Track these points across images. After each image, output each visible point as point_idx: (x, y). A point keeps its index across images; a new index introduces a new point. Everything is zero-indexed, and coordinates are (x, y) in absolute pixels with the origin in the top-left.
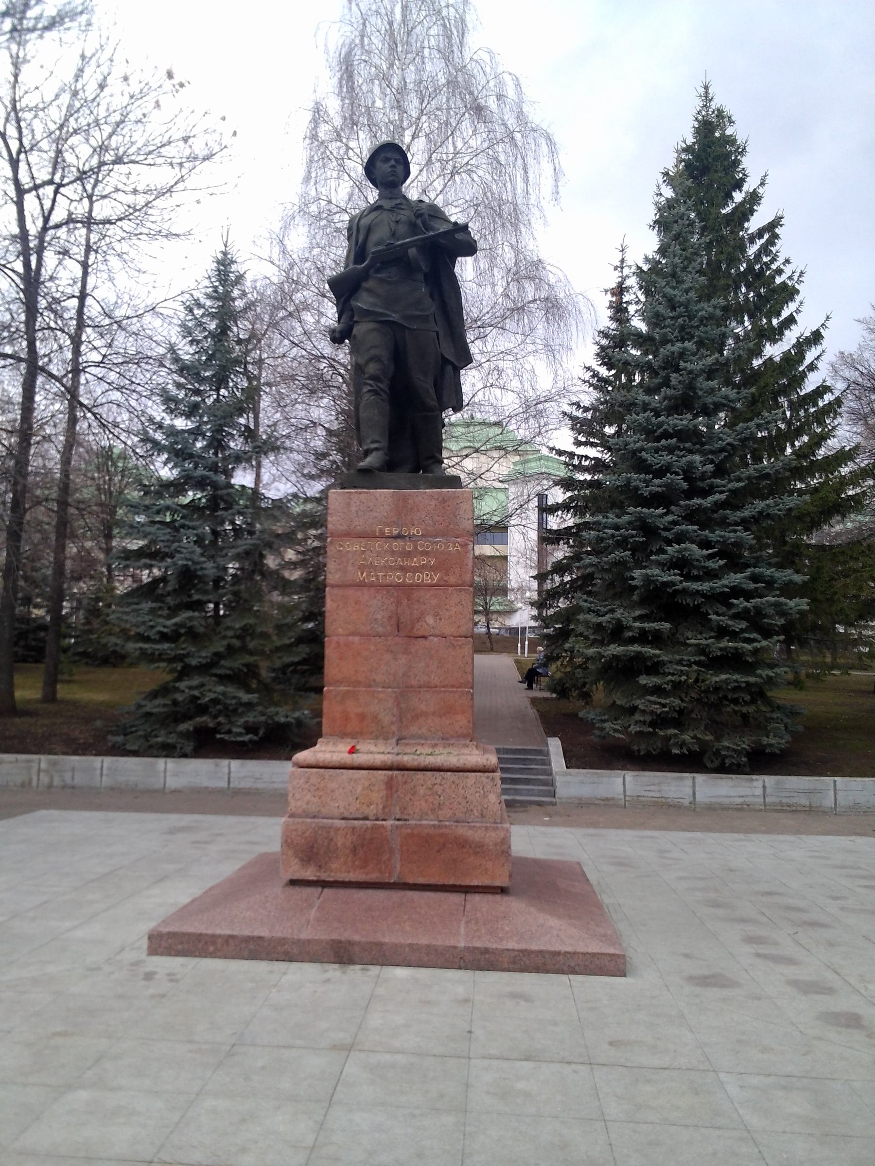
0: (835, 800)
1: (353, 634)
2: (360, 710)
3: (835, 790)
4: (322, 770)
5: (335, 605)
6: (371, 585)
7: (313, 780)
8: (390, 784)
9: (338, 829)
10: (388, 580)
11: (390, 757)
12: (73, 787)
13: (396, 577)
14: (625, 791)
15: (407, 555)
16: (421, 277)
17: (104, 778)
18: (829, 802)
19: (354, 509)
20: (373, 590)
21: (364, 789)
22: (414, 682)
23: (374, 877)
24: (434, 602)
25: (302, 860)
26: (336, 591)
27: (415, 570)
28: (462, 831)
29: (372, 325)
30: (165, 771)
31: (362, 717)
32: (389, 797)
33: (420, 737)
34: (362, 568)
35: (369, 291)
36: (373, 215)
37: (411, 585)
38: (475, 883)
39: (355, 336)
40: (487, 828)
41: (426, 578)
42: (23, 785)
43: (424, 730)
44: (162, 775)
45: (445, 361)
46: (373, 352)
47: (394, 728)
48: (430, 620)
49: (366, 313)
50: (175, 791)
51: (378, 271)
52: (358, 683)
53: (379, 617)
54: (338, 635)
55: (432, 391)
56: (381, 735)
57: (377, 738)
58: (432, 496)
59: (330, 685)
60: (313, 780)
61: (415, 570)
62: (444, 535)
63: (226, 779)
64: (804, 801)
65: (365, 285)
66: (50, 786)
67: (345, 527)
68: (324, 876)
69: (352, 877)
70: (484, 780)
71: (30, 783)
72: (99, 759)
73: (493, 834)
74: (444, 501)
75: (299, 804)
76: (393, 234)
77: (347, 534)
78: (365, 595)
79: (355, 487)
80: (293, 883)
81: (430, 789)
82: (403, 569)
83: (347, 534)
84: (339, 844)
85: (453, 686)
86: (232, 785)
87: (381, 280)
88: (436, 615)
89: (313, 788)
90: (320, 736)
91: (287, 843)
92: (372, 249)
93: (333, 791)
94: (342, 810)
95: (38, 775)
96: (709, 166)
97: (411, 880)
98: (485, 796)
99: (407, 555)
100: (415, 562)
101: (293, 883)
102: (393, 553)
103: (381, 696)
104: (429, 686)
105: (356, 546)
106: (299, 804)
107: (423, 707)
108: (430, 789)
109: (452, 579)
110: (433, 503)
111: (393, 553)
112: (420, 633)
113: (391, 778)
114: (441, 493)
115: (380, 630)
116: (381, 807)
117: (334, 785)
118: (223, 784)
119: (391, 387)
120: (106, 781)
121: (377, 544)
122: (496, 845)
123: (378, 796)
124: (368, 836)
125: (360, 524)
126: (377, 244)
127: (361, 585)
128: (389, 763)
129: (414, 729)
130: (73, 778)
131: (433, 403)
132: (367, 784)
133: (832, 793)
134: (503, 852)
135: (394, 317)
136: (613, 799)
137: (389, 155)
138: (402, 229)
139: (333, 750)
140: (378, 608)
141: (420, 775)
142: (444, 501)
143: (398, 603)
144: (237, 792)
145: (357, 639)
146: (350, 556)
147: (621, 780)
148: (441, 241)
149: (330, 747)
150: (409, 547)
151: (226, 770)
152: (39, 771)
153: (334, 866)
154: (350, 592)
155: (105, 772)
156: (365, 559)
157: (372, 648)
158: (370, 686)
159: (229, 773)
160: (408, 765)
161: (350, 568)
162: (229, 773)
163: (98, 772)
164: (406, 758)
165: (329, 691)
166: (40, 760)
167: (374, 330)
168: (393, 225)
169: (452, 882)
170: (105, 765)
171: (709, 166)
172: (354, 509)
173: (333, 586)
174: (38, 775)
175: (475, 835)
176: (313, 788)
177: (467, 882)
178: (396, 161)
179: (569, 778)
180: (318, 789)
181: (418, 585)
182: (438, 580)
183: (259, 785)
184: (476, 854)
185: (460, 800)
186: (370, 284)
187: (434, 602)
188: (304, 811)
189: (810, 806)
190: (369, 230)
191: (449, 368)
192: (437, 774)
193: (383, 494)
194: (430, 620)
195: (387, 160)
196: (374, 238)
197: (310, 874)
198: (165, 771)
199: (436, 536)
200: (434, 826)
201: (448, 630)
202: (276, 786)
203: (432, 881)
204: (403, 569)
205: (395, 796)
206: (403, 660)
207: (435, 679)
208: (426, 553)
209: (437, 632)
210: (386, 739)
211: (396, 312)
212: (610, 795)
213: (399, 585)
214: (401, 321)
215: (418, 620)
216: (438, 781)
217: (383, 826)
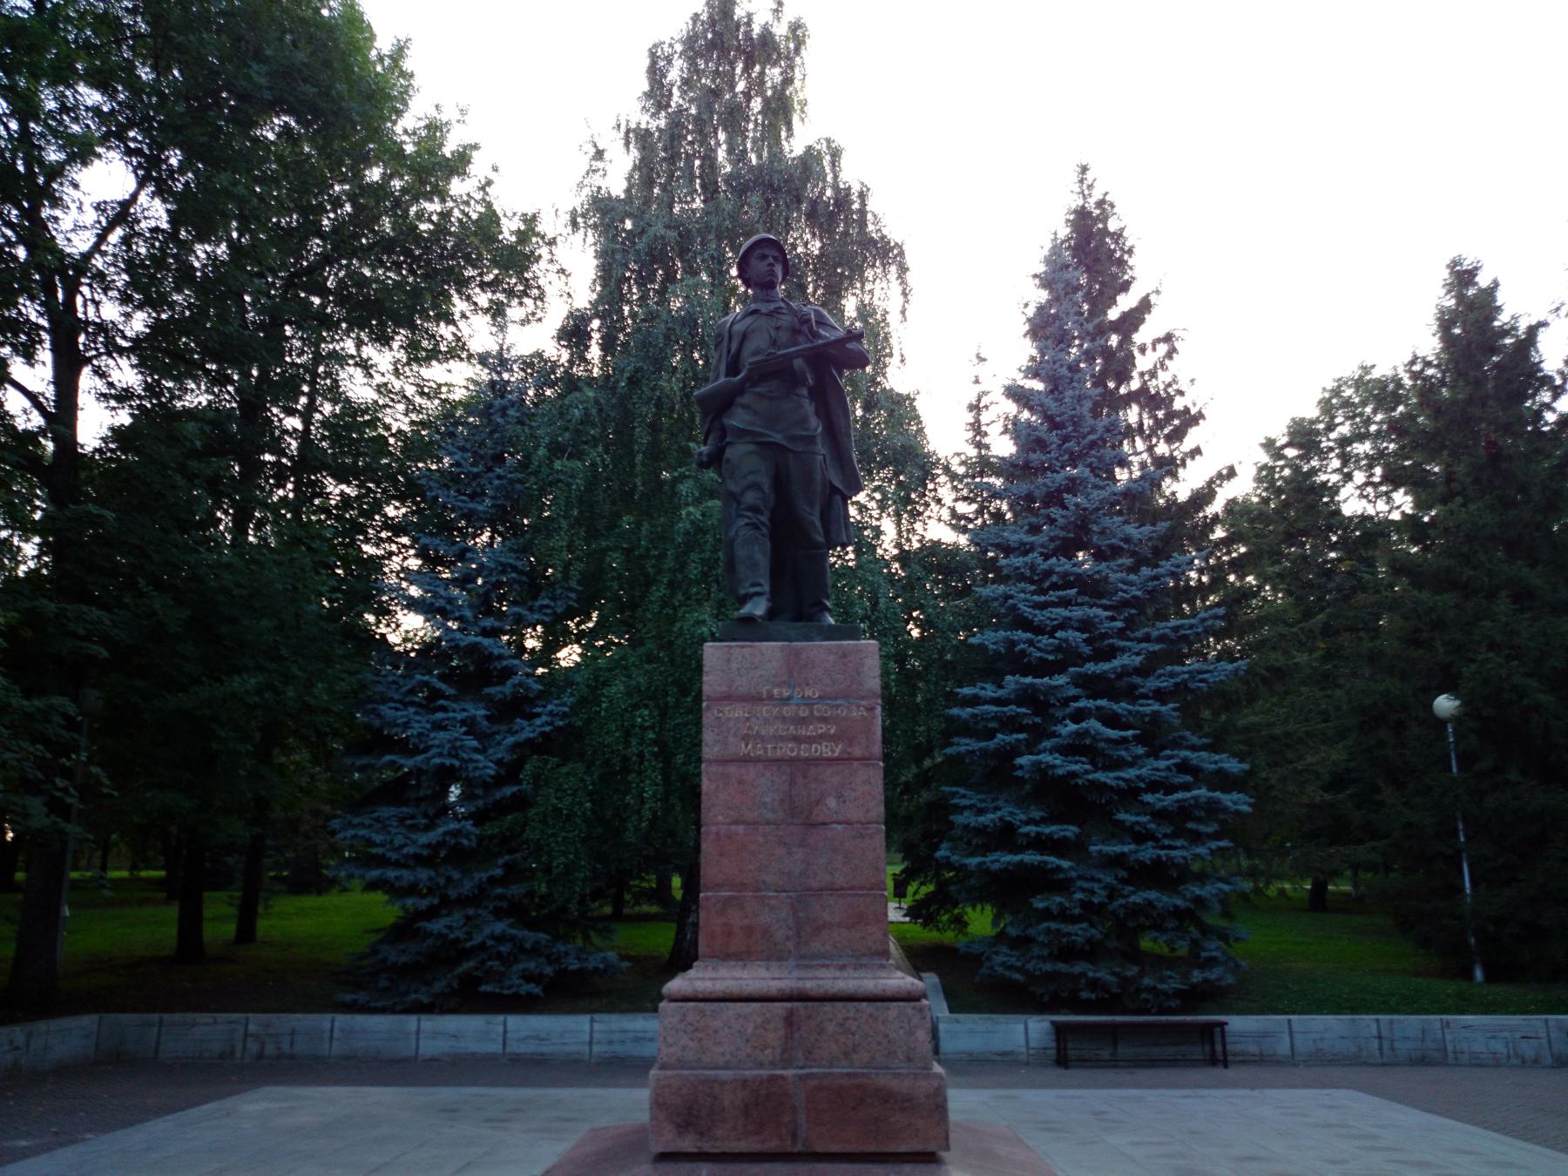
0: (1292, 1045)
1: (736, 822)
2: (746, 922)
3: (1291, 1033)
4: (701, 1005)
5: (713, 786)
6: (757, 760)
7: (691, 1018)
8: (789, 1021)
9: (723, 1083)
10: (779, 753)
11: (772, 983)
12: (292, 1057)
13: (787, 750)
14: (1027, 1041)
15: (803, 722)
16: (805, 392)
17: (335, 1043)
18: (1283, 1048)
19: (734, 666)
20: (760, 766)
21: (756, 1028)
22: (815, 884)
23: (772, 1145)
24: (836, 780)
25: (678, 1126)
26: (714, 769)
27: (810, 740)
28: (884, 1080)
29: (751, 447)
30: (418, 1031)
31: (749, 931)
32: (788, 1038)
33: (823, 956)
34: (746, 738)
35: (746, 407)
36: (749, 320)
37: (807, 759)
38: (903, 1148)
39: (728, 461)
40: (916, 1075)
41: (825, 750)
42: (221, 1056)
43: (828, 947)
44: (413, 1037)
45: (834, 490)
46: (751, 478)
47: (790, 945)
48: (832, 803)
49: (742, 433)
50: (432, 1059)
51: (754, 384)
52: (743, 886)
53: (768, 799)
54: (716, 824)
55: (818, 524)
56: (773, 955)
57: (768, 959)
58: (829, 651)
59: (708, 889)
60: (691, 1018)
61: (810, 740)
62: (845, 697)
63: (500, 1040)
64: (1253, 1049)
65: (739, 400)
66: (260, 1056)
67: (724, 689)
68: (707, 1147)
69: (743, 1146)
70: (910, 1011)
71: (232, 1053)
72: (328, 1017)
73: (924, 1083)
74: (844, 656)
75: (672, 1050)
76: (774, 343)
77: (728, 698)
78: (751, 772)
79: (734, 640)
80: (664, 1157)
81: (841, 1025)
82: (797, 739)
83: (728, 698)
84: (726, 1103)
85: (862, 888)
86: (508, 1050)
87: (760, 394)
88: (839, 797)
89: (690, 1029)
90: (696, 958)
91: (658, 1104)
92: (748, 359)
93: (716, 1032)
94: (728, 1057)
95: (245, 1042)
96: (1090, 259)
97: (819, 1148)
98: (911, 1033)
99: (803, 722)
100: (811, 731)
101: (664, 1157)
102: (784, 719)
103: (773, 902)
104: (832, 889)
105: (738, 712)
106: (672, 1050)
107: (826, 916)
108: (841, 1025)
109: (857, 752)
110: (831, 658)
111: (784, 719)
112: (820, 819)
113: (791, 1013)
114: (839, 647)
115: (770, 816)
116: (779, 1050)
117: (716, 1024)
118: (496, 1047)
119: (771, 520)
120: (337, 1049)
121: (764, 710)
122: (928, 1097)
123: (774, 1036)
124: (763, 1092)
125: (743, 685)
126: (756, 353)
127: (745, 760)
128: (788, 991)
129: (815, 946)
130: (292, 1044)
131: (821, 539)
132: (759, 1020)
133: (1286, 1038)
134: (938, 1106)
135: (778, 438)
136: (1012, 1053)
137: (766, 251)
138: (784, 336)
139: (714, 975)
140: (767, 788)
141: (827, 1007)
142: (844, 656)
143: (792, 783)
144: (517, 1060)
145: (741, 829)
146: (731, 724)
147: (1021, 1027)
148: (831, 351)
149: (710, 974)
150: (804, 712)
151: (501, 1029)
152: (246, 1034)
153: (719, 1133)
154: (732, 769)
155: (336, 1035)
156: (749, 728)
157: (760, 839)
158: (758, 890)
159: (505, 1032)
160: (813, 994)
161: (731, 739)
162: (505, 1032)
163: (327, 1035)
164: (809, 985)
165: (707, 898)
166: (247, 1020)
167: (751, 453)
168: (773, 334)
169: (873, 1148)
170: (337, 1024)
171: (1090, 259)
172: (734, 666)
173: (710, 762)
174: (245, 1042)
175: (900, 1086)
176: (690, 1029)
177: (891, 1148)
178: (775, 258)
179: (957, 1027)
180: (697, 1030)
181: (816, 759)
182: (842, 752)
183: (544, 1049)
184: (903, 1110)
185: (879, 1038)
186: (746, 399)
187: (836, 780)
188: (679, 1061)
189: (1261, 1054)
190: (744, 337)
191: (838, 498)
192: (850, 1005)
193: (771, 650)
194: (832, 803)
195: (764, 257)
196: (749, 347)
197: (688, 1144)
198: (418, 1031)
199: (836, 698)
200: (848, 1074)
201: (855, 814)
202: (567, 1049)
203: (850, 1148)
204: (797, 739)
205: (797, 1036)
206: (799, 854)
207: (841, 880)
208: (824, 720)
209: (841, 818)
210: (780, 959)
211: (778, 432)
212: (1009, 1048)
213: (791, 760)
214: (783, 442)
215: (817, 803)
216: (851, 1014)
217: (782, 1077)
